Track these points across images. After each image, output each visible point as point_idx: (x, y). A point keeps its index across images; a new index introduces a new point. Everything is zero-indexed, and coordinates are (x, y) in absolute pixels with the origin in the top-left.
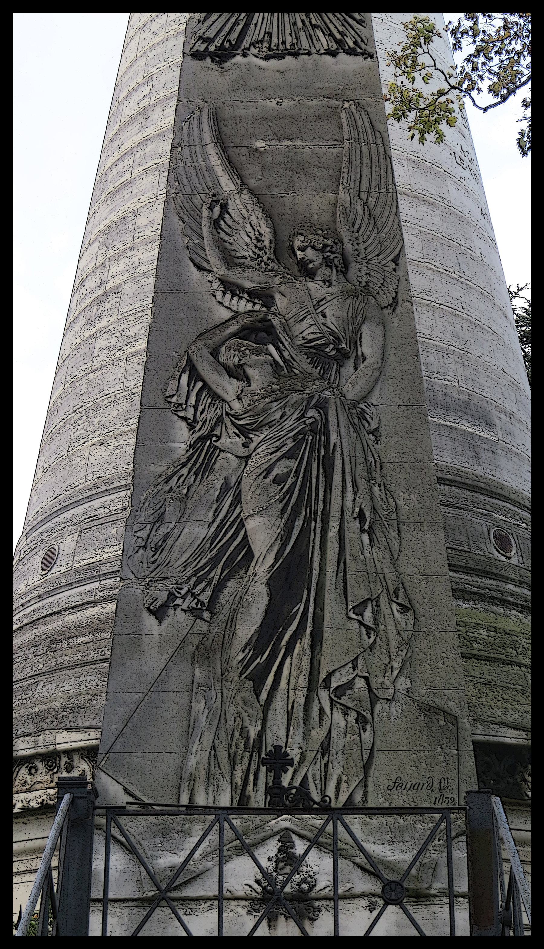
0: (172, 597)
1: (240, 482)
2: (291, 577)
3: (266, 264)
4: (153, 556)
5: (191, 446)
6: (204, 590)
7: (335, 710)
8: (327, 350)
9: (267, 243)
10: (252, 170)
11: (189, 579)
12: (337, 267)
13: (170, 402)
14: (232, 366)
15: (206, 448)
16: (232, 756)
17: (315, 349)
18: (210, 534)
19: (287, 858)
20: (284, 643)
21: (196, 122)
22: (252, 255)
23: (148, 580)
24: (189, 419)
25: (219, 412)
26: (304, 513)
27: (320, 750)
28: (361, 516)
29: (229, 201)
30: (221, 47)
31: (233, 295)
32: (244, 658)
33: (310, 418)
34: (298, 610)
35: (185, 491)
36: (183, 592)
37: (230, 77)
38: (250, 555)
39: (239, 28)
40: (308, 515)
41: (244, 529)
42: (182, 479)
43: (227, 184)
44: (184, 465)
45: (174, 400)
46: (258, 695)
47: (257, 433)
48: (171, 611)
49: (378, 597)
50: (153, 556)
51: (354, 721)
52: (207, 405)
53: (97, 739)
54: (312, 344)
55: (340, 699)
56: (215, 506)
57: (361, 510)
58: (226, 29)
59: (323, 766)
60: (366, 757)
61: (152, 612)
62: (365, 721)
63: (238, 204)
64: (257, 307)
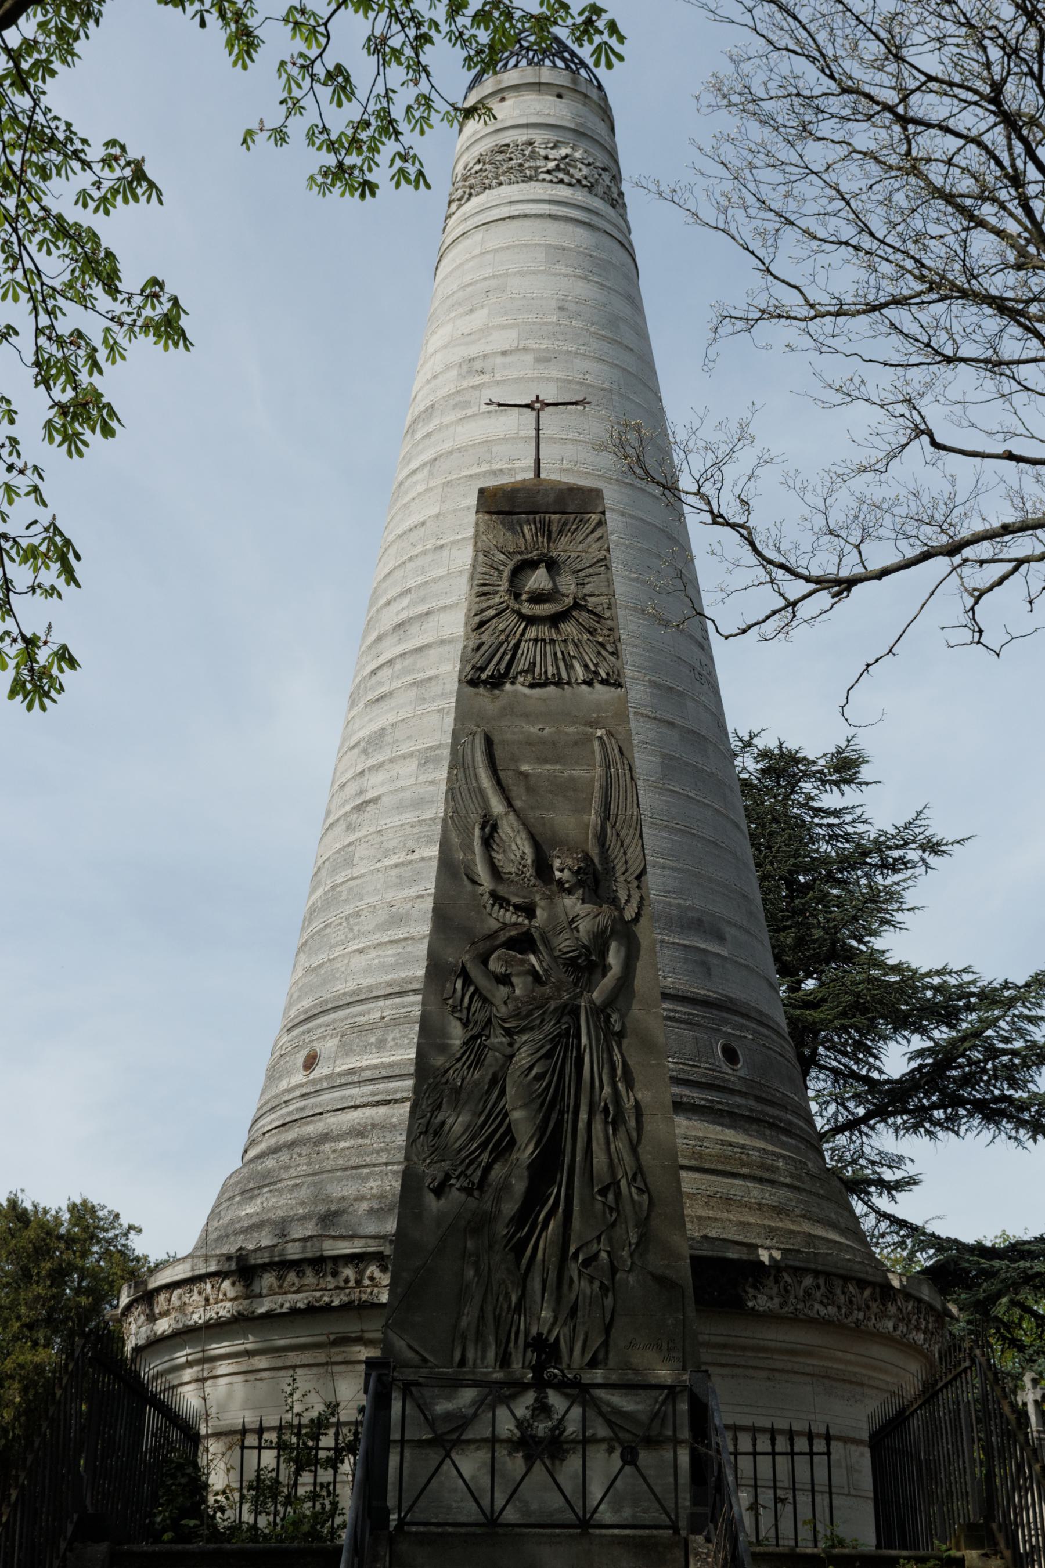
2: (545, 1169)
5: (464, 1043)
9: (529, 861)
11: (463, 1161)
19: (542, 1409)
30: (492, 676)
31: (501, 907)
37: (499, 704)
38: (513, 1142)
39: (508, 657)
43: (497, 806)
45: (450, 1001)
48: (447, 1189)
57: (606, 1104)
58: (496, 659)
60: (607, 1321)
61: (432, 1190)
63: (508, 828)
64: (520, 919)
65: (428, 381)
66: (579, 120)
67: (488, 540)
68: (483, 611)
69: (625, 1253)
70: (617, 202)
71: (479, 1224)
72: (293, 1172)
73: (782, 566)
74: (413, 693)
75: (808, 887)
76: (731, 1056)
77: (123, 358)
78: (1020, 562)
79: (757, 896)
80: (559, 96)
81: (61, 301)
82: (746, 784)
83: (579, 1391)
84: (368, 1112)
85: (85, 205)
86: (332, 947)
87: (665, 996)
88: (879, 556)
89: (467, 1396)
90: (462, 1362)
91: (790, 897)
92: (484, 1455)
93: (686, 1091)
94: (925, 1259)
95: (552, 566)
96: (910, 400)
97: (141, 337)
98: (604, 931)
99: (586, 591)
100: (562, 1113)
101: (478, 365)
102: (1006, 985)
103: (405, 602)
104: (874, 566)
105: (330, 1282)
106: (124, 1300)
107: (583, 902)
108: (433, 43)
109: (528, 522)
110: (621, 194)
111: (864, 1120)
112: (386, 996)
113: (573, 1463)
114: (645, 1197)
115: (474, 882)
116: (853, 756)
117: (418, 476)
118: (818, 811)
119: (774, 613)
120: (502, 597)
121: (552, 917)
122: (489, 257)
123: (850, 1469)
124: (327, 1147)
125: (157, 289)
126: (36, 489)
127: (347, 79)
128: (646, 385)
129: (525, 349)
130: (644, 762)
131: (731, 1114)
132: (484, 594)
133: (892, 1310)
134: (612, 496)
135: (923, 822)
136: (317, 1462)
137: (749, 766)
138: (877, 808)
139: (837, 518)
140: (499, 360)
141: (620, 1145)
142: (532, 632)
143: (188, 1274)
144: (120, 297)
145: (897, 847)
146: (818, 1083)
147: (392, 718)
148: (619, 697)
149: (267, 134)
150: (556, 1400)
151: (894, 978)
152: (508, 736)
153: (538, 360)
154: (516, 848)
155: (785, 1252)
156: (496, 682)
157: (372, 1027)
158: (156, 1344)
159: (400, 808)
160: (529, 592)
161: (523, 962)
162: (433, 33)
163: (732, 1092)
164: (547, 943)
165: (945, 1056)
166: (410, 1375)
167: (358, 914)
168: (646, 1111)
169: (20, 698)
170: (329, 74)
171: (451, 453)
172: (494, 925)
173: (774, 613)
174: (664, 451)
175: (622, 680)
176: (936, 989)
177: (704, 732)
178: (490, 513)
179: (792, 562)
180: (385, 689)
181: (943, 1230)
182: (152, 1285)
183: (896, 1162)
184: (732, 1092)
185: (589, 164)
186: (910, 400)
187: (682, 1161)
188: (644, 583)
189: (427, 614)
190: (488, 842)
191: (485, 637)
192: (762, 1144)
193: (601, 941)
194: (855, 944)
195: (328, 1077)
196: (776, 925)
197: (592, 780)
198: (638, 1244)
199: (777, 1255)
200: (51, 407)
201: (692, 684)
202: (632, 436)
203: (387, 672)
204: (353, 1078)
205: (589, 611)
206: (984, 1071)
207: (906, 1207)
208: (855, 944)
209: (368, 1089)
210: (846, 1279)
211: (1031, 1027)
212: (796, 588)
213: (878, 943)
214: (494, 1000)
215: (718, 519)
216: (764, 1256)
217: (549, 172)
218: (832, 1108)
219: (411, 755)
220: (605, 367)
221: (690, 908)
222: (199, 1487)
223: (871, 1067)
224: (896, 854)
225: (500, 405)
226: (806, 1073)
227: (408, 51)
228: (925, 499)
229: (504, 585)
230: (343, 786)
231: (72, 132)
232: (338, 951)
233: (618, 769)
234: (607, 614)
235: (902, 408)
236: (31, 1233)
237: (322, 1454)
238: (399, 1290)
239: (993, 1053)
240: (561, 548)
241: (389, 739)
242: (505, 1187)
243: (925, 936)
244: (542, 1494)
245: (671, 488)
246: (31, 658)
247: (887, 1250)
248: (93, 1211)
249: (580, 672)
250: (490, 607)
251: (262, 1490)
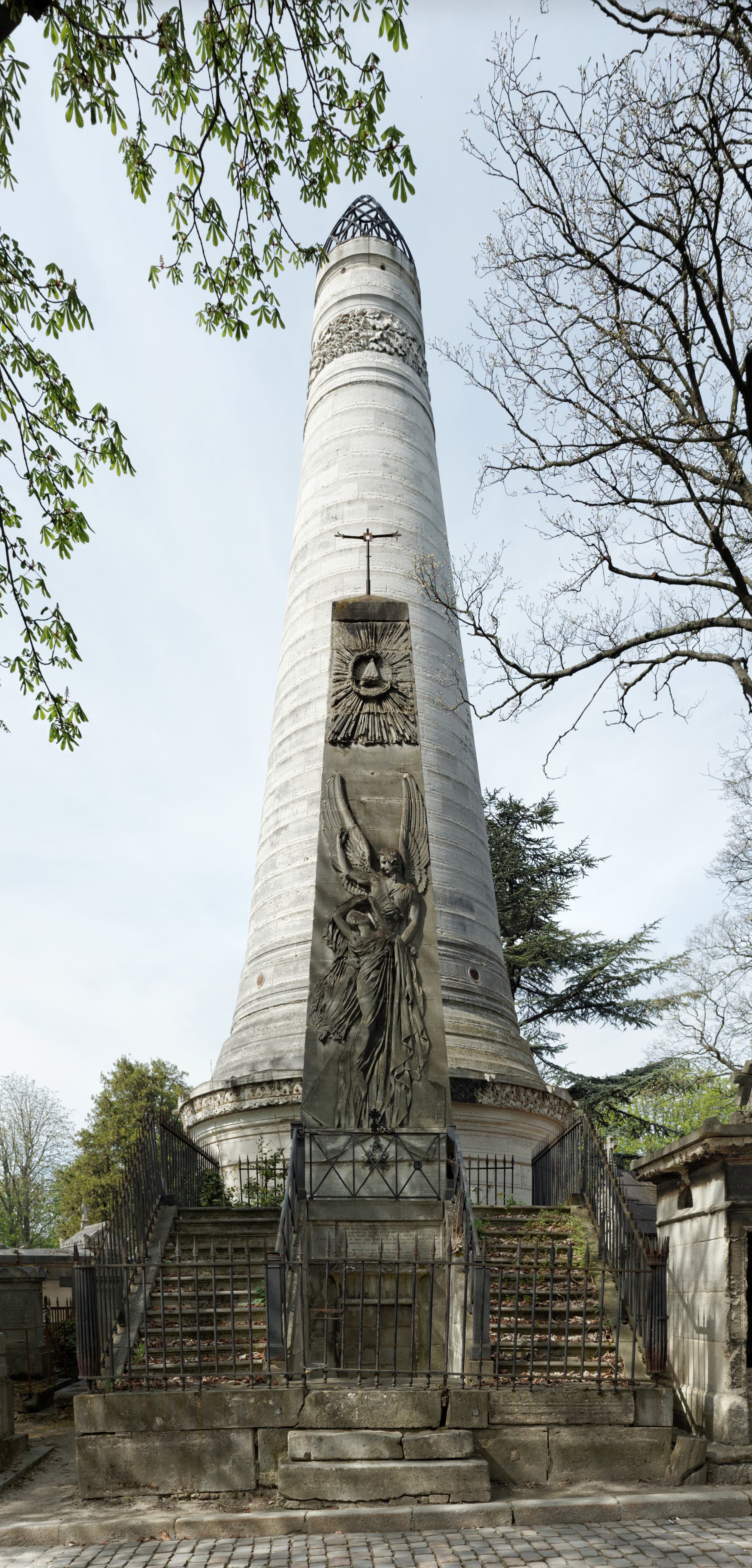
2: (378, 1026)
10: (359, 813)
19: (378, 1146)
28: (408, 997)
30: (344, 738)
38: (361, 1015)
43: (349, 823)
53: (300, 1001)
63: (355, 837)
65: (303, 526)
66: (397, 292)
67: (340, 642)
68: (337, 693)
69: (417, 1071)
70: (421, 370)
71: (345, 1058)
72: (256, 1039)
73: (515, 666)
74: (303, 757)
75: (520, 885)
76: (474, 974)
77: (91, 481)
78: (654, 663)
79: (491, 884)
80: (383, 268)
81: (43, 429)
82: (491, 823)
83: (394, 1135)
84: (291, 1006)
85: (39, 327)
86: (268, 916)
87: (440, 942)
88: (573, 658)
89: (342, 1140)
90: (339, 1126)
91: (511, 891)
92: (350, 1168)
93: (451, 994)
94: (566, 1085)
95: (378, 661)
96: (598, 533)
97: (101, 462)
99: (398, 679)
100: (385, 999)
101: (333, 513)
102: (618, 943)
103: (295, 695)
104: (568, 666)
105: (277, 1093)
106: (180, 1104)
108: (279, 173)
109: (363, 628)
110: (424, 363)
111: (541, 1015)
112: (298, 944)
113: (392, 1171)
115: (337, 870)
116: (550, 805)
117: (300, 601)
118: (529, 840)
119: (509, 700)
120: (348, 683)
121: (380, 891)
122: (337, 419)
123: (523, 1177)
124: (271, 1025)
125: (102, 414)
126: (42, 583)
127: (219, 216)
128: (438, 530)
129: (362, 499)
130: (432, 802)
131: (474, 1006)
132: (338, 681)
133: (547, 1103)
134: (414, 614)
136: (275, 1175)
137: (492, 812)
138: (558, 839)
139: (550, 632)
140: (346, 508)
141: (415, 1016)
142: (367, 708)
143: (208, 1091)
144: (79, 422)
145: (570, 862)
146: (520, 996)
147: (292, 774)
149: (166, 271)
150: (383, 1142)
151: (561, 938)
152: (354, 778)
153: (371, 508)
154: (360, 850)
155: (497, 1075)
156: (346, 743)
157: (291, 960)
158: (197, 1124)
159: (299, 832)
161: (365, 917)
162: (278, 161)
163: (474, 994)
164: (377, 907)
165: (584, 982)
166: (313, 1131)
167: (280, 897)
168: (428, 998)
169: (56, 740)
170: (206, 209)
171: (318, 583)
172: (349, 896)
173: (509, 700)
174: (448, 585)
176: (584, 946)
177: (466, 783)
178: (340, 621)
179: (521, 664)
180: (287, 755)
181: (576, 1072)
182: (192, 1097)
183: (555, 1037)
184: (474, 994)
185: (403, 335)
186: (598, 533)
187: (447, 1030)
188: (435, 680)
189: (309, 703)
190: (344, 846)
191: (339, 711)
192: (489, 1022)
193: (405, 905)
194: (542, 918)
195: (269, 989)
196: (502, 907)
197: (401, 806)
199: (493, 1077)
200: (44, 516)
201: (460, 752)
202: (428, 568)
203: (287, 744)
204: (282, 989)
205: (400, 693)
206: (603, 989)
207: (558, 1059)
208: (542, 918)
209: (291, 994)
210: (526, 1088)
211: (628, 964)
212: (522, 682)
213: (554, 918)
215: (479, 631)
216: (487, 1077)
217: (376, 341)
218: (527, 1009)
219: (304, 798)
220: (413, 515)
221: (456, 892)
222: (219, 1186)
223: (548, 988)
224: (568, 866)
225: (345, 537)
226: (514, 991)
227: (261, 180)
228: (603, 616)
229: (350, 675)
230: (267, 819)
231: (19, 252)
232: (271, 918)
233: (416, 800)
234: (410, 696)
235: (593, 539)
236: (134, 1075)
237: (278, 1172)
239: (608, 979)
241: (291, 788)
242: (358, 1038)
243: (582, 915)
244: (376, 1184)
245: (451, 608)
246: (60, 712)
247: (551, 1083)
248: (164, 1065)
249: (394, 736)
251: (250, 1188)
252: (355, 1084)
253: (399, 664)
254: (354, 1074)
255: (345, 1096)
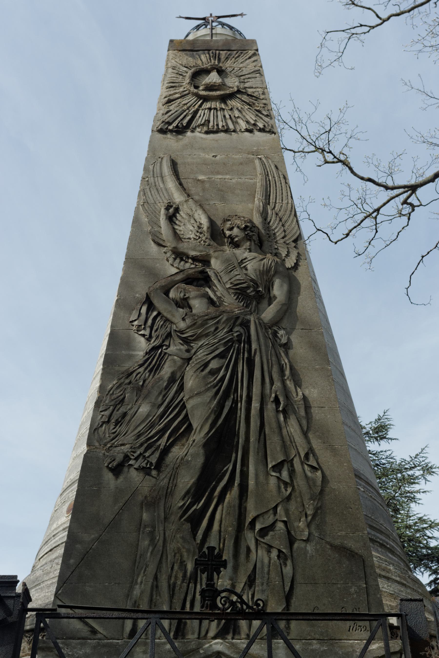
0: (127, 458)
1: (183, 377)
2: (222, 442)
3: (204, 242)
4: (114, 428)
5: (147, 353)
6: (153, 453)
7: (259, 548)
8: (248, 291)
9: (205, 229)
12: (255, 241)
13: (133, 325)
14: (178, 300)
15: (158, 354)
16: (171, 587)
17: (240, 290)
18: (159, 413)
20: (217, 493)
21: (158, 164)
22: (195, 237)
23: (109, 445)
24: (146, 335)
25: (168, 329)
26: (232, 397)
27: (247, 583)
28: (277, 401)
29: (180, 206)
31: (182, 260)
32: (184, 504)
33: (237, 332)
34: (229, 467)
35: (141, 383)
36: (136, 455)
37: (181, 143)
38: (190, 428)
40: (235, 399)
41: (186, 410)
42: (139, 375)
43: (178, 197)
44: (141, 366)
45: (136, 323)
46: (194, 535)
47: (196, 342)
48: (126, 469)
49: (293, 459)
50: (114, 428)
51: (276, 558)
52: (160, 326)
54: (238, 287)
55: (264, 539)
56: (163, 393)
59: (250, 597)
60: (287, 589)
62: (286, 559)
68: (170, 95)
69: (302, 524)
95: (221, 72)
98: (269, 270)
100: (235, 402)
107: (250, 251)
114: (319, 473)
135: (424, 455)
138: (398, 449)
142: (208, 105)
148: (273, 139)
160: (205, 85)
168: (313, 404)
175: (275, 130)
191: (171, 108)
197: (255, 184)
198: (314, 516)
214: (174, 320)
224: (410, 473)
238: (72, 561)
240: (228, 65)
249: (243, 125)
250: (176, 93)
252: (172, 546)
253: (247, 76)
254: (172, 527)
255: (152, 569)
